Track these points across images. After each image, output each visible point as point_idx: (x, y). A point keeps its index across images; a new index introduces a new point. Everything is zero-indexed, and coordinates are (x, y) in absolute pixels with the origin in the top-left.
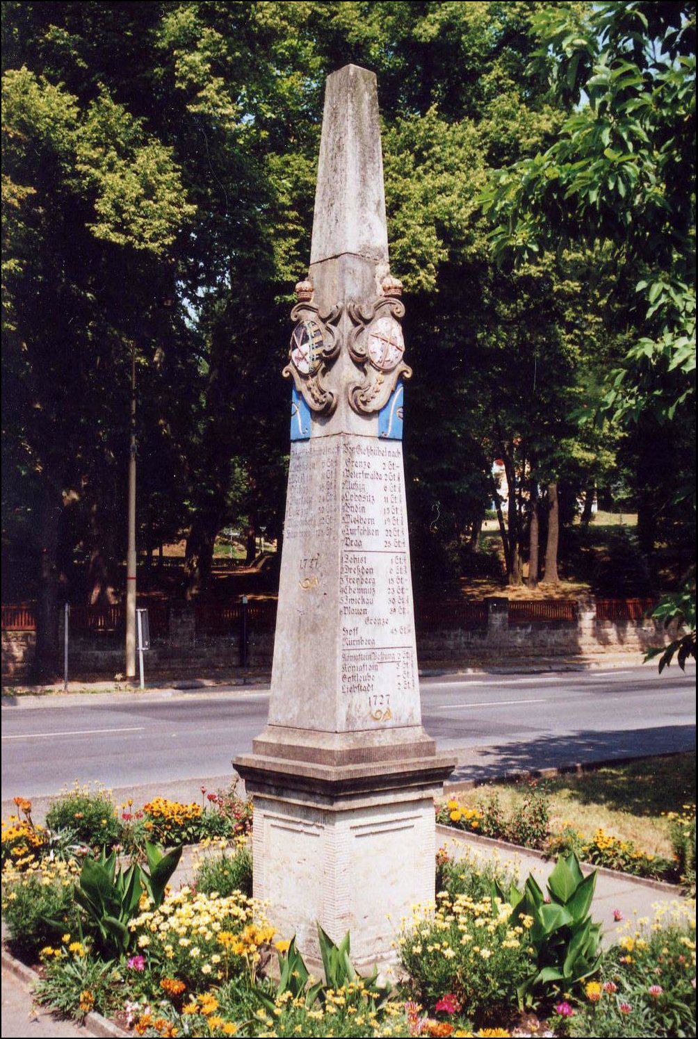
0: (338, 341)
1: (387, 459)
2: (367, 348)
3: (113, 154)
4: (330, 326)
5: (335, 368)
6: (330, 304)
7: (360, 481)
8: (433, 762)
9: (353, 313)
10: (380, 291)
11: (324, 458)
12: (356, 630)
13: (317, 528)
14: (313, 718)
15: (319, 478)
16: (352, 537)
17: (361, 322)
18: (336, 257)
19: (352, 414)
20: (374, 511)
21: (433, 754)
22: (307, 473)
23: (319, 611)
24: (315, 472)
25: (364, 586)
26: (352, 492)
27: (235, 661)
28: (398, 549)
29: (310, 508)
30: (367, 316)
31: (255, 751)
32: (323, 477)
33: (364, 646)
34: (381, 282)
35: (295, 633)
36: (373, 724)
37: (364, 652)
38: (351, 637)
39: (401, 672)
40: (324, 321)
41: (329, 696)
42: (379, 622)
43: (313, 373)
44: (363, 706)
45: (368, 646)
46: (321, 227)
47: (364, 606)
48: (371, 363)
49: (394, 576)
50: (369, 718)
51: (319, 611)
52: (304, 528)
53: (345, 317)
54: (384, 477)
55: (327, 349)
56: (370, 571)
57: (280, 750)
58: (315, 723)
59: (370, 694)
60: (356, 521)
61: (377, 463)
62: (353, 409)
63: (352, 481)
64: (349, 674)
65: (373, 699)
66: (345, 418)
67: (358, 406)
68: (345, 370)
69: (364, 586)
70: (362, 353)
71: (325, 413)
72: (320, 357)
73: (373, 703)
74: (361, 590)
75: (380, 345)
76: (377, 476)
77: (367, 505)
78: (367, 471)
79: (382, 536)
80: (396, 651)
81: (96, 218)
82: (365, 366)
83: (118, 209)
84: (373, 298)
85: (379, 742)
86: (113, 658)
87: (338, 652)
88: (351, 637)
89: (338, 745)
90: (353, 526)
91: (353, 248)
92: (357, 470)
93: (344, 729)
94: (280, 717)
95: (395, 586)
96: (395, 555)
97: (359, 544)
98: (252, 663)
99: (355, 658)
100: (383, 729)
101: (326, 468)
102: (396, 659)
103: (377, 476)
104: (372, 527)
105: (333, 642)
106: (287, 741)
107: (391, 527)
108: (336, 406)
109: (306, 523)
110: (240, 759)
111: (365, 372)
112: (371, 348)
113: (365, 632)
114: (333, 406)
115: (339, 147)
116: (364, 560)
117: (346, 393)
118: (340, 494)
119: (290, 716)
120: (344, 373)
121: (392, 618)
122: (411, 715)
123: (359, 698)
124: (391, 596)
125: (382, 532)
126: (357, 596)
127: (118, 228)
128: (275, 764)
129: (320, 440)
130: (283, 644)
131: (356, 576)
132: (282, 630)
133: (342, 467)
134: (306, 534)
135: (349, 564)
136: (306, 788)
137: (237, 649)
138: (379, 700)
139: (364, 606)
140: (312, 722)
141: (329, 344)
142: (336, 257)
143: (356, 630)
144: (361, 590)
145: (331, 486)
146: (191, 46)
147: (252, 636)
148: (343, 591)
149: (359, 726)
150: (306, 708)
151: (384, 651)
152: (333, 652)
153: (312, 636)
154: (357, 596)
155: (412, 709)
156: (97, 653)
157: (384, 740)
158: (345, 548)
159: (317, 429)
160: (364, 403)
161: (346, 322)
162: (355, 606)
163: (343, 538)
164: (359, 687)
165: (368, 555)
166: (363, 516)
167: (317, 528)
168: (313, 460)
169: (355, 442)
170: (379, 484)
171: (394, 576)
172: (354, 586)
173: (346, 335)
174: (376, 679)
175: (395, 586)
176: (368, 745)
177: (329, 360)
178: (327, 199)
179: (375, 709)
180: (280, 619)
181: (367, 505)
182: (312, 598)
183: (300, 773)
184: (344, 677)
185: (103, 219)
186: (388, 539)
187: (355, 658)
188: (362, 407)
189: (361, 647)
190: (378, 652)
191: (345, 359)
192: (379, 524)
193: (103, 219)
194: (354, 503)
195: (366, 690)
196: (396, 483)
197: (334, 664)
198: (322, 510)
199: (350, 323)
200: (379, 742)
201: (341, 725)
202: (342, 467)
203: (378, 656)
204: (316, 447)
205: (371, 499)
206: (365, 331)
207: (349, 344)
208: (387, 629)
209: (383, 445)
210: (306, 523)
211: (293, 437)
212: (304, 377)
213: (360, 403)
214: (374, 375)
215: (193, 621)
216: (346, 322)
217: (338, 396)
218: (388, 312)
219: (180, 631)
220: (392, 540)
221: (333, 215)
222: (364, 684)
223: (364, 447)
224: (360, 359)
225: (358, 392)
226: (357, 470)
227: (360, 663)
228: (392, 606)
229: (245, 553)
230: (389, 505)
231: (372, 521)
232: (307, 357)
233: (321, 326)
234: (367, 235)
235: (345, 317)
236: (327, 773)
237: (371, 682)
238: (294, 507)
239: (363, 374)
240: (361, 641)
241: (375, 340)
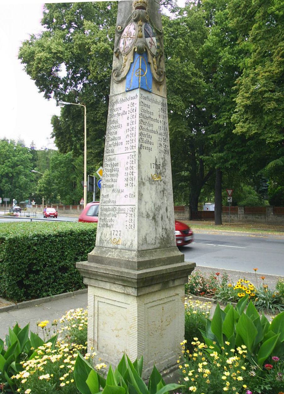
56: (117, 165)
59: (112, 229)
69: (114, 173)
104: (119, 141)
116: (114, 159)
124: (126, 177)
125: (124, 143)
171: (129, 165)
181: (119, 130)
190: (117, 207)
192: (123, 140)
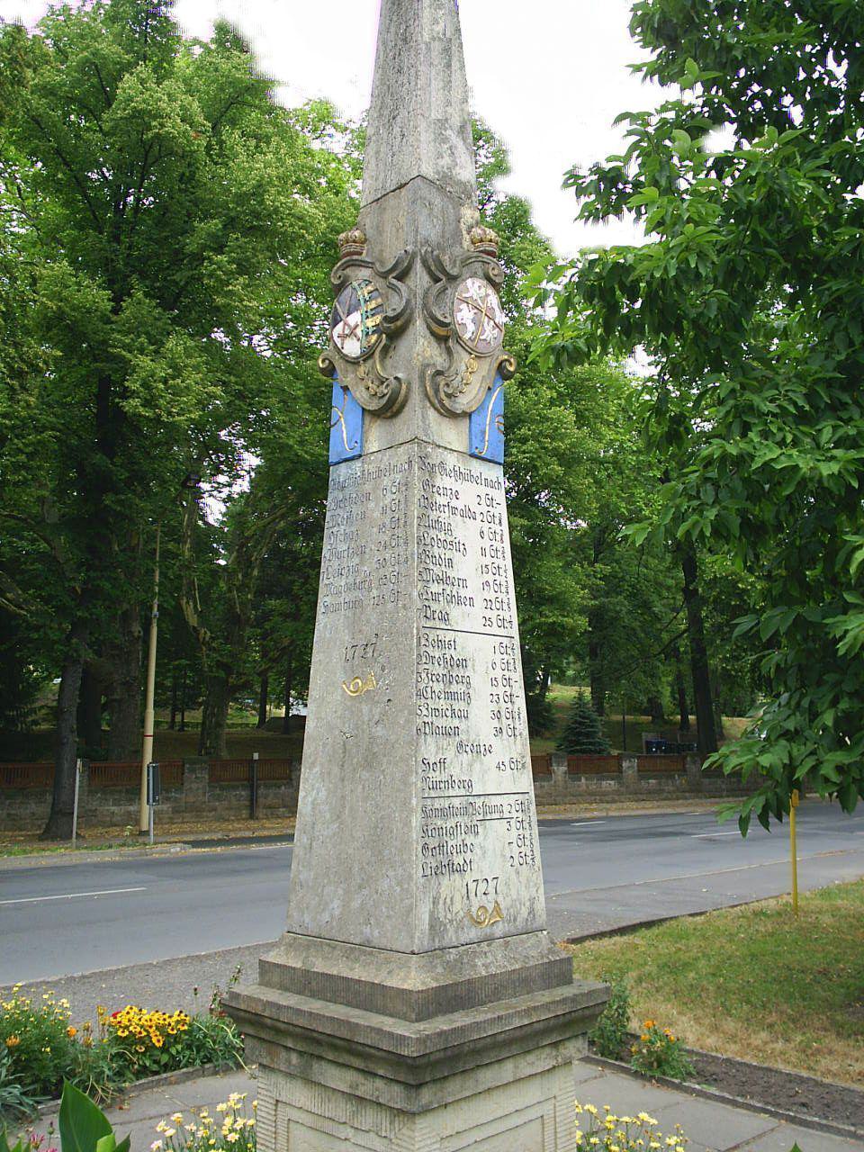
0: (408, 302)
1: (483, 490)
2: (452, 315)
3: (143, 339)
4: (394, 281)
5: (403, 345)
6: (392, 249)
7: (445, 516)
8: (574, 999)
9: (431, 262)
10: (466, 243)
11: (386, 481)
12: (443, 762)
13: (375, 593)
14: (367, 922)
15: (377, 514)
16: (434, 606)
17: (443, 277)
18: (401, 187)
19: (432, 414)
20: (467, 567)
21: (569, 982)
22: (356, 510)
23: (379, 731)
24: (372, 505)
25: (454, 688)
26: (433, 533)
27: (245, 813)
28: (502, 632)
29: (362, 563)
30: (454, 272)
31: (264, 983)
32: (384, 512)
33: (457, 792)
34: (469, 233)
35: (336, 770)
36: (473, 934)
37: (456, 802)
38: (436, 776)
39: (514, 833)
40: (384, 275)
41: (399, 884)
42: (480, 750)
43: (367, 355)
44: (457, 898)
45: (463, 792)
46: (377, 152)
47: (456, 722)
48: (458, 339)
49: (498, 673)
50: (466, 921)
51: (379, 731)
52: (349, 597)
53: (418, 266)
54: (479, 517)
55: (391, 314)
56: (463, 663)
57: (307, 983)
58: (374, 934)
59: (469, 877)
60: (440, 580)
61: (469, 494)
62: (433, 405)
63: (434, 515)
64: (433, 843)
65: (472, 886)
66: (419, 417)
67: (441, 401)
68: (419, 346)
70: (447, 321)
71: (390, 409)
72: (378, 330)
73: (472, 895)
74: (451, 696)
75: (471, 315)
76: (468, 514)
77: (457, 557)
78: (454, 503)
79: (479, 610)
80: (504, 800)
81: (126, 394)
82: (450, 343)
83: (145, 385)
84: (457, 251)
85: (486, 966)
86: (129, 813)
87: (414, 802)
88: (436, 776)
89: (414, 979)
90: (435, 588)
91: (428, 170)
92: (442, 500)
93: (426, 945)
94: (307, 919)
95: (500, 690)
96: (501, 639)
97: (445, 618)
98: (261, 816)
99: (444, 813)
100: (490, 939)
101: (389, 497)
102: (506, 815)
103: (468, 514)
104: (463, 593)
105: (405, 783)
106: (320, 966)
107: (492, 596)
108: (403, 406)
109: (355, 586)
110: (235, 996)
111: (449, 352)
112: (459, 316)
113: (458, 766)
114: (400, 399)
115: (405, 40)
116: (452, 644)
117: (422, 377)
118: (419, 537)
119: (326, 917)
120: (418, 348)
121: (496, 743)
122: (532, 911)
123: (450, 886)
124: (494, 707)
125: (479, 603)
126: (442, 704)
127: (147, 403)
128: (299, 1012)
129: (379, 455)
130: (313, 787)
131: (441, 671)
132: (313, 764)
133: (417, 492)
134: (356, 605)
135: (430, 650)
136: (357, 1062)
137: (248, 803)
138: (482, 887)
139: (456, 722)
140: (367, 930)
141: (395, 305)
142: (401, 187)
143: (443, 762)
144: (451, 696)
145: (399, 522)
146: (220, 250)
147: (262, 791)
148: (420, 694)
149: (451, 937)
150: (356, 904)
151: (487, 800)
152: (406, 803)
153: (365, 775)
154: (442, 704)
155: (532, 900)
156: (113, 808)
157: (491, 963)
158: (424, 622)
159: (376, 437)
160: (449, 396)
161: (419, 278)
162: (440, 722)
163: (420, 606)
164: (450, 864)
165: (460, 637)
166: (451, 573)
167: (375, 593)
168: (368, 487)
169: (436, 456)
170: (474, 526)
172: (438, 687)
173: (420, 292)
174: (477, 850)
175: (500, 690)
176: (468, 974)
177: (393, 331)
178: (386, 112)
179: (476, 903)
180: (308, 748)
181: (457, 557)
182: (365, 708)
183: (346, 1034)
184: (425, 847)
185: (134, 394)
186: (488, 614)
187: (444, 813)
188: (446, 402)
189: (451, 793)
190: (479, 802)
191: (419, 325)
192: (473, 589)
193: (134, 394)
194: (436, 551)
195: (461, 871)
196: (498, 528)
197: (407, 824)
198: (383, 563)
199: (426, 278)
200: (486, 966)
201: (421, 939)
202: (417, 492)
203: (477, 812)
204: (372, 468)
205: (461, 548)
206: (449, 291)
207: (425, 306)
208: (491, 761)
209: (477, 467)
210: (355, 586)
211: (332, 459)
212: (355, 362)
213: (443, 395)
214: (463, 360)
215: (207, 777)
216: (419, 278)
217: (409, 384)
218: (480, 273)
219: (194, 786)
220: (493, 615)
221: (397, 130)
222: (458, 860)
223: (449, 467)
224: (441, 331)
225: (440, 378)
226: (442, 500)
227: (451, 823)
228: (496, 723)
229: (258, 718)
230: (488, 560)
231: (463, 582)
232: (359, 332)
233: (380, 283)
234: (446, 161)
235: (418, 266)
236: (402, 1039)
237: (468, 856)
238: (335, 563)
239: (445, 356)
240: (450, 783)
241: (464, 306)
